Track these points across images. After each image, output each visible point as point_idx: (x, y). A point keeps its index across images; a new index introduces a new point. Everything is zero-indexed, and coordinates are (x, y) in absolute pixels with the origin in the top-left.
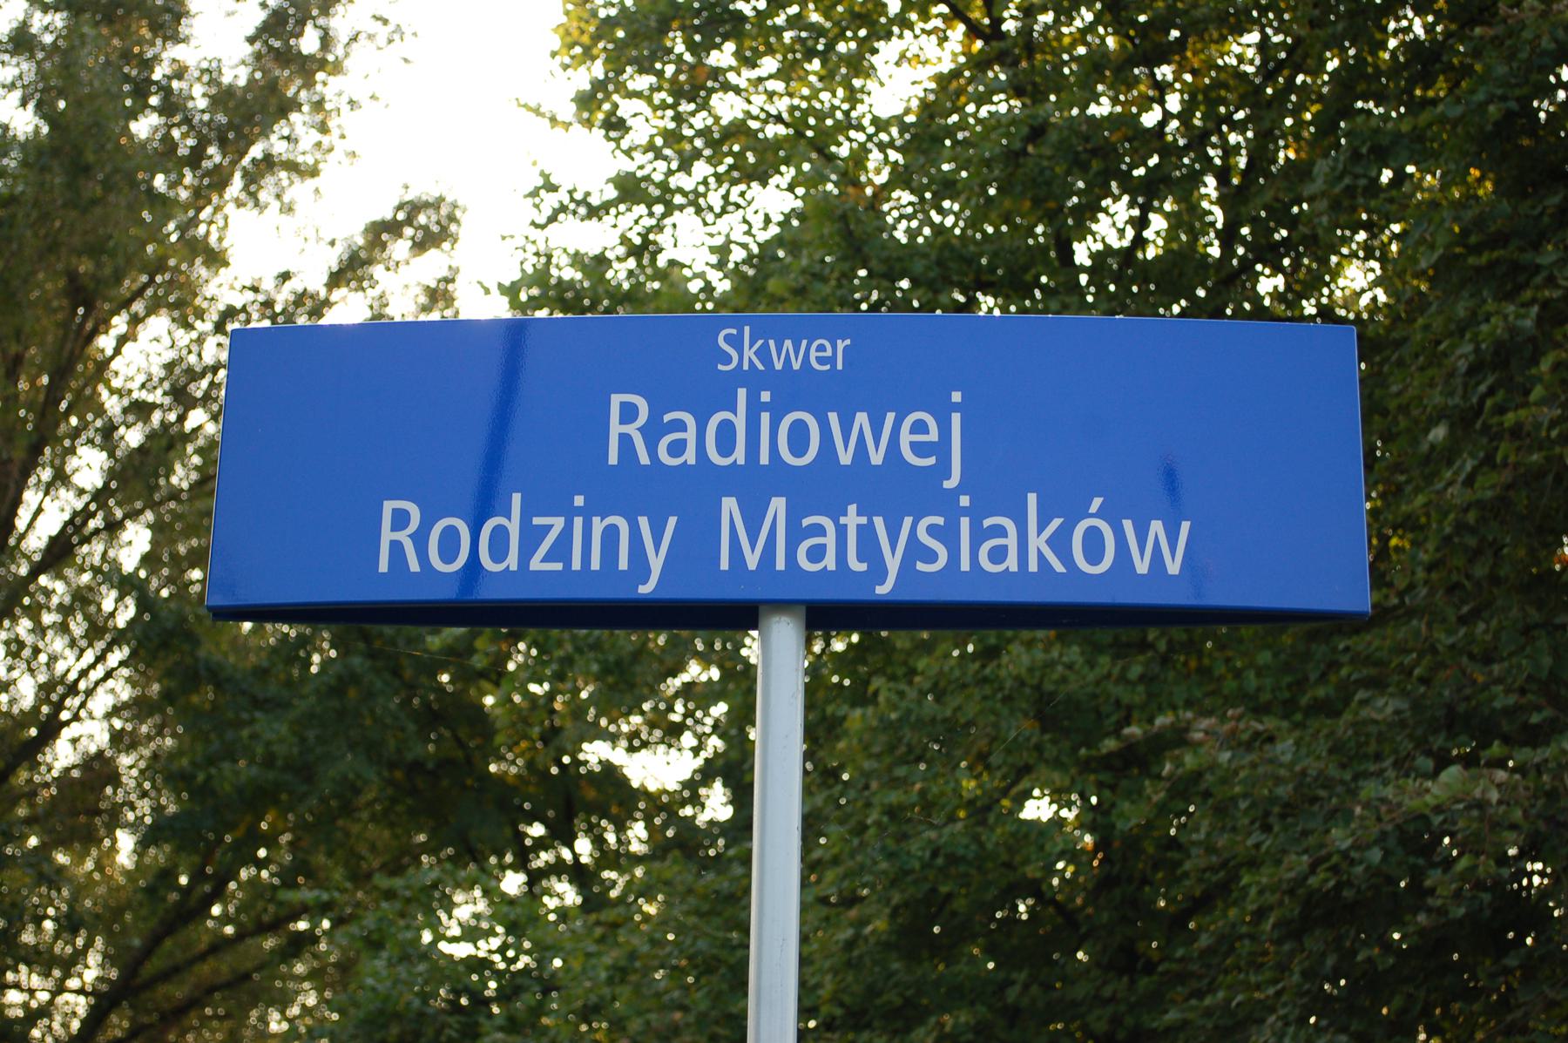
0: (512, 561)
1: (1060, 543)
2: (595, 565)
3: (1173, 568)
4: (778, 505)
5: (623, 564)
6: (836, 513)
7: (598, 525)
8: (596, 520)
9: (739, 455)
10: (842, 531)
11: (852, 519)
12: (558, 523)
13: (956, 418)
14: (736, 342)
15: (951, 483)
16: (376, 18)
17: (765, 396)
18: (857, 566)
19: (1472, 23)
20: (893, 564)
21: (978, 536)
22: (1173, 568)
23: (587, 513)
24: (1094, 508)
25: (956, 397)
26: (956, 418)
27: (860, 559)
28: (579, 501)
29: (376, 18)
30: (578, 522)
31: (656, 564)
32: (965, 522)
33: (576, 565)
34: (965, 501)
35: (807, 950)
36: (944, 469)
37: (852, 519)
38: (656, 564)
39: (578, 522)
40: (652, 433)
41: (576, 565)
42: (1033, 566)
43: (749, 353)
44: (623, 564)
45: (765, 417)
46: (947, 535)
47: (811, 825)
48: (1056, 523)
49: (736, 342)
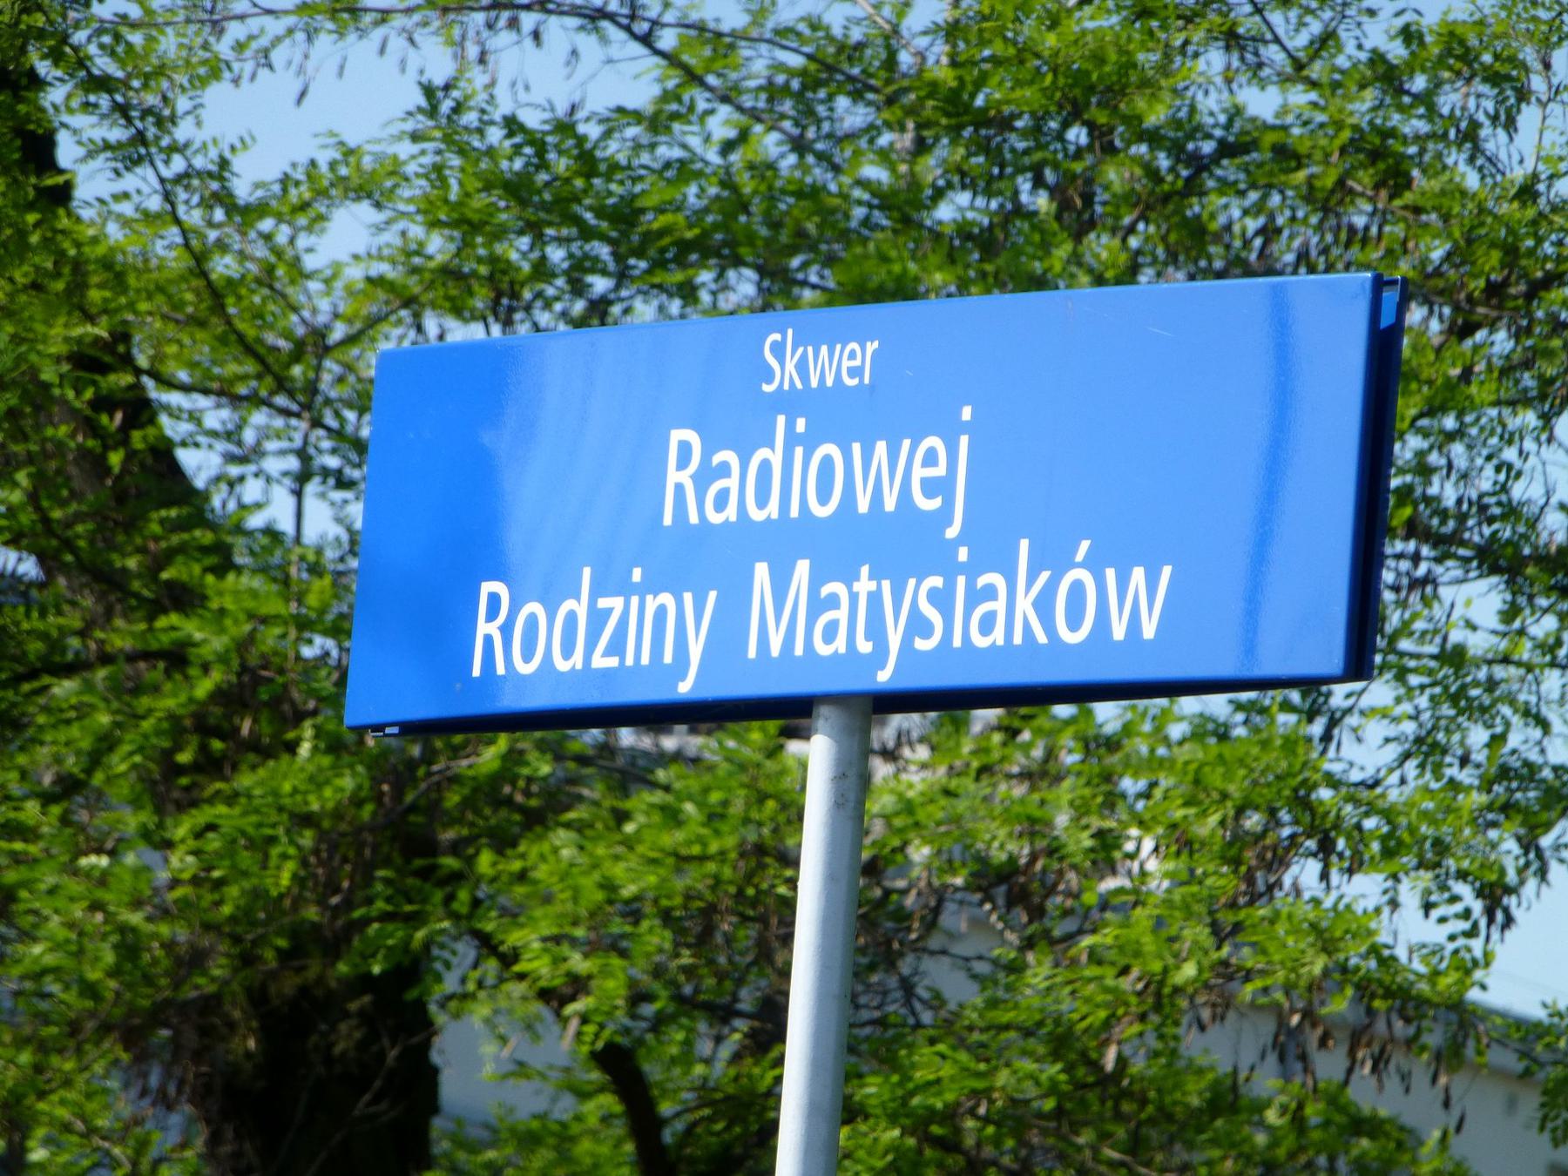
0: (577, 660)
1: (1044, 606)
2: (645, 660)
3: (1149, 631)
4: (803, 568)
5: (668, 658)
6: (850, 578)
7: (651, 604)
8: (649, 598)
9: (773, 509)
10: (854, 598)
11: (864, 586)
12: (616, 603)
13: (964, 440)
14: (778, 350)
15: (952, 532)
16: (403, 70)
17: (801, 424)
18: (865, 647)
19: (881, 207)
20: (894, 641)
21: (974, 597)
22: (1149, 631)
23: (644, 589)
24: (1079, 557)
25: (966, 413)
26: (964, 440)
27: (867, 638)
28: (637, 574)
29: (403, 70)
30: (635, 600)
31: (696, 651)
32: (961, 581)
33: (629, 661)
34: (963, 554)
35: (776, 1072)
36: (945, 515)
37: (864, 586)
38: (696, 651)
39: (635, 600)
40: (705, 477)
41: (629, 661)
42: (1018, 639)
43: (790, 366)
44: (668, 658)
45: (799, 451)
46: (942, 600)
47: (787, 939)
48: (1045, 576)
49: (778, 350)
